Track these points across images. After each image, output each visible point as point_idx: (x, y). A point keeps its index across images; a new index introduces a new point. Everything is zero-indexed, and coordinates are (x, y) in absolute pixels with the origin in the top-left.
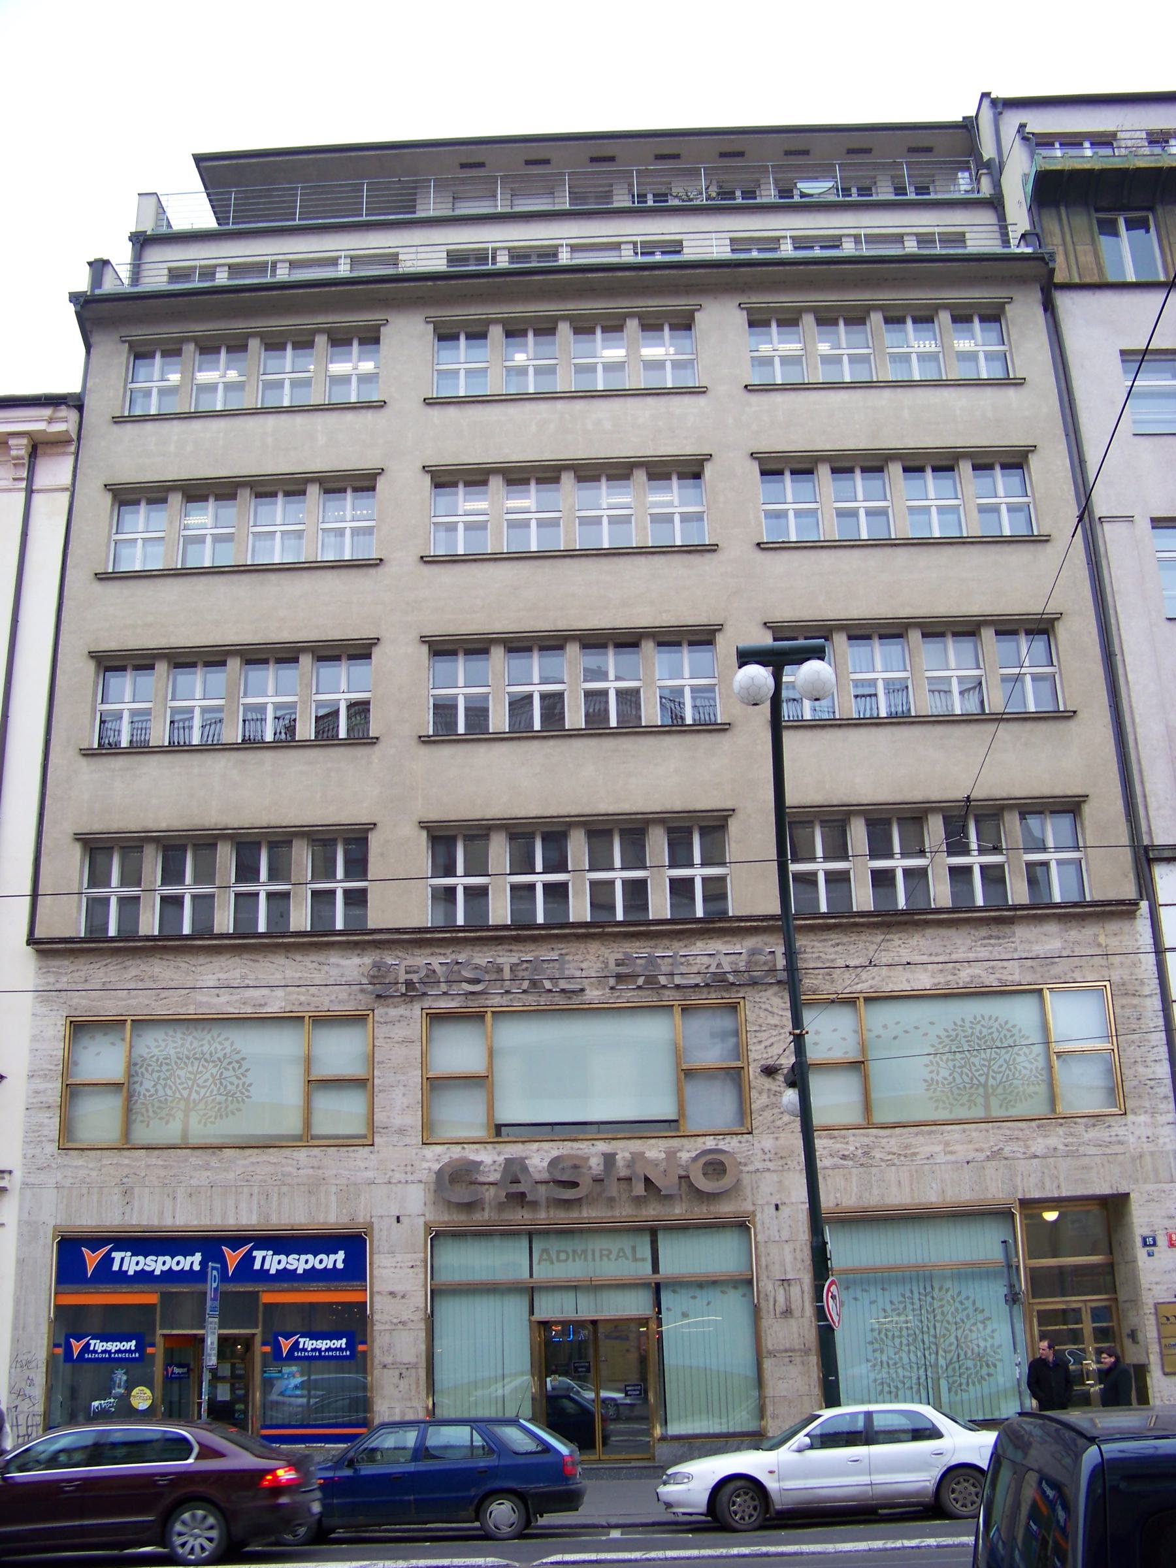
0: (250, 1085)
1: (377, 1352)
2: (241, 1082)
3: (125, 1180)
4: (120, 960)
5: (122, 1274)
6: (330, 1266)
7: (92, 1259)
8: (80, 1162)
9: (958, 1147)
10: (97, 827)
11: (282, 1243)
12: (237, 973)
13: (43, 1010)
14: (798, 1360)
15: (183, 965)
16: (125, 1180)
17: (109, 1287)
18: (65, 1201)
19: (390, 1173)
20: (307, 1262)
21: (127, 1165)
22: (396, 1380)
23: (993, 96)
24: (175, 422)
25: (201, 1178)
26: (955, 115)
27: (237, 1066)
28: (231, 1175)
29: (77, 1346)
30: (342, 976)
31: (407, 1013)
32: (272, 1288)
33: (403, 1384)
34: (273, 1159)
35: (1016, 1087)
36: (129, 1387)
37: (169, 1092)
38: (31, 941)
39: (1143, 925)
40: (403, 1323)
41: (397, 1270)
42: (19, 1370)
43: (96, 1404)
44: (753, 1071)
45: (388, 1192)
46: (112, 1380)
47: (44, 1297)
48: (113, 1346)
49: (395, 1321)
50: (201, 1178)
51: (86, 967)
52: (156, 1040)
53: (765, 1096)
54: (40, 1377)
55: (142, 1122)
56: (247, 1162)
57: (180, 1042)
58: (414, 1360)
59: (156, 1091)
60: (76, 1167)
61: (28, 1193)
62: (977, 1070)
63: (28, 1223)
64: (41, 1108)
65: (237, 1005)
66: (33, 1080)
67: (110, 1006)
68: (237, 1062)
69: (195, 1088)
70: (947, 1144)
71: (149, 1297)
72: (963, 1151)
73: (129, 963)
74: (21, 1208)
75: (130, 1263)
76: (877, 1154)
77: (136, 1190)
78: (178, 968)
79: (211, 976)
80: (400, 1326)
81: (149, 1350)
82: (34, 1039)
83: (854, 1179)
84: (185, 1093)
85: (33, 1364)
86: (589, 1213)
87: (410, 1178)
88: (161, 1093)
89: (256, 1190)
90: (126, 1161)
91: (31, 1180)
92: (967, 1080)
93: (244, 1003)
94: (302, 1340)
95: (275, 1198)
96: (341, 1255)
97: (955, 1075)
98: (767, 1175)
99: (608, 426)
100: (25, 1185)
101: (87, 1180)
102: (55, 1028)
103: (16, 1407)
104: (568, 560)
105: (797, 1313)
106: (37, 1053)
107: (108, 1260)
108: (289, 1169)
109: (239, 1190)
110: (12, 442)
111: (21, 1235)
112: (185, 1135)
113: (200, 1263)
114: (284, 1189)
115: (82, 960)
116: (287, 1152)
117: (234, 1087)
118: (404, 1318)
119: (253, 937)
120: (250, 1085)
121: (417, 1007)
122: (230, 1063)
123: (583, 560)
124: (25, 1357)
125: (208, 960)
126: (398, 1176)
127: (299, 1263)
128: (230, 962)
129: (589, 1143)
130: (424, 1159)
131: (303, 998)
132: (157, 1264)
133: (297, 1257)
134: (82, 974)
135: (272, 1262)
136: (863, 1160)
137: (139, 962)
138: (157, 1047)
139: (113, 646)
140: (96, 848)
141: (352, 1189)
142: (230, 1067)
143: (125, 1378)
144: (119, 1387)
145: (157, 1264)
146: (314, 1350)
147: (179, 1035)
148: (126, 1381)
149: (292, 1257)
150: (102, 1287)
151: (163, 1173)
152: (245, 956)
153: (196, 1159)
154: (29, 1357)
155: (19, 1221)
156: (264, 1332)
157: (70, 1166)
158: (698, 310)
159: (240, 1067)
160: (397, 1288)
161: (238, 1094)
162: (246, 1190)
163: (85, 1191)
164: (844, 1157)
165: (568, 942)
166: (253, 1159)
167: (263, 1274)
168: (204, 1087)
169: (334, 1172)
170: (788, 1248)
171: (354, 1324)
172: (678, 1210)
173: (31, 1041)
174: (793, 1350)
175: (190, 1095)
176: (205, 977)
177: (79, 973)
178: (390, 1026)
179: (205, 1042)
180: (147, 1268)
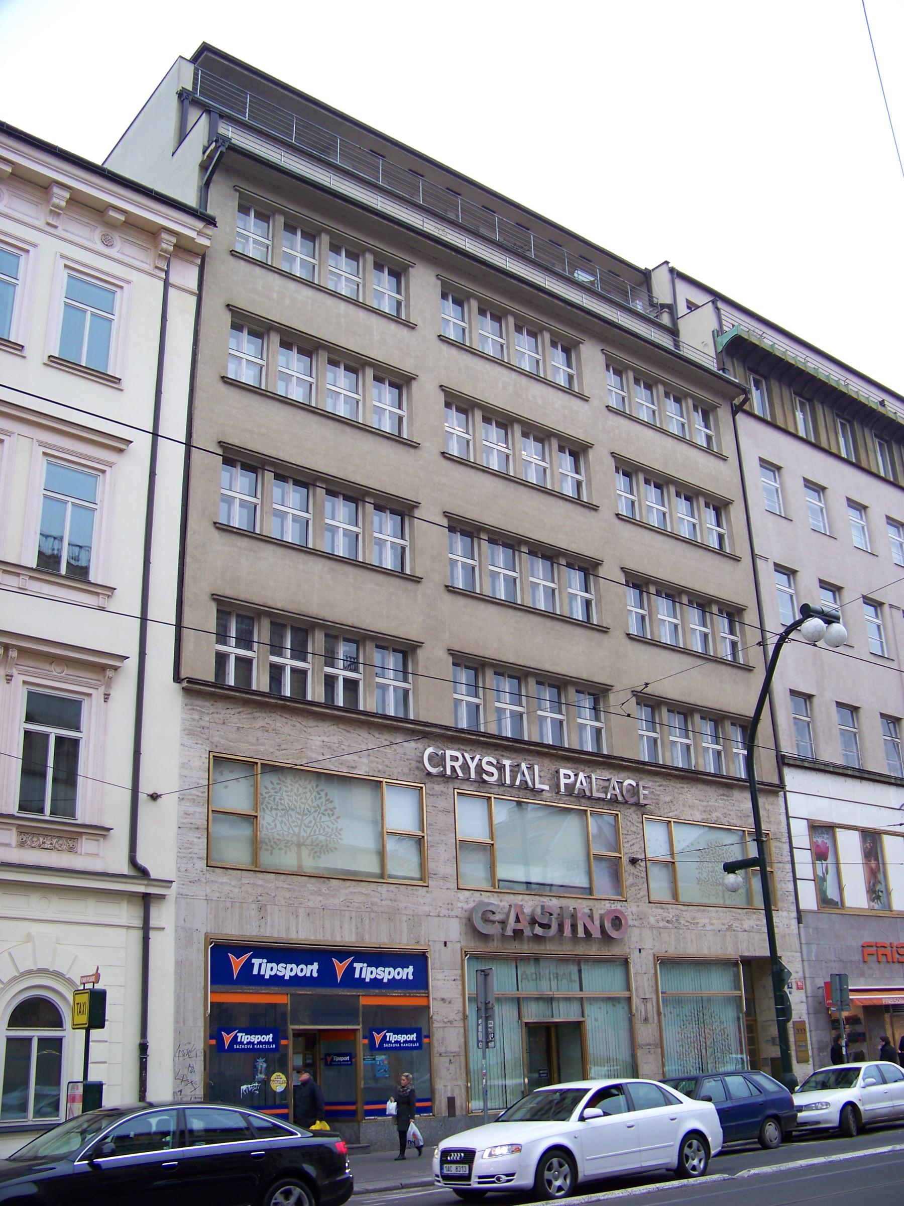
0: (341, 830)
1: (436, 1044)
2: (334, 827)
3: (260, 898)
4: (250, 711)
5: (260, 977)
6: (308, 975)
7: (237, 963)
8: (225, 880)
9: (715, 921)
10: (229, 593)
11: (377, 958)
12: (335, 739)
13: (189, 742)
14: (652, 1051)
15: (297, 724)
16: (260, 898)
17: (252, 989)
18: (213, 912)
19: (439, 909)
20: (291, 970)
21: (262, 886)
22: (447, 1065)
23: (670, 265)
24: (277, 276)
25: (315, 901)
26: (642, 263)
27: (331, 813)
28: (336, 901)
29: (227, 1038)
30: (405, 754)
31: (445, 790)
32: (368, 993)
33: (452, 1068)
34: (364, 891)
35: (321, 842)
36: (269, 1073)
37: (285, 828)
38: (177, 678)
39: (781, 800)
40: (451, 1022)
41: (446, 982)
42: (181, 1058)
43: (244, 1087)
44: (625, 861)
45: (436, 924)
46: (255, 1067)
47: (200, 995)
48: (255, 1039)
49: (446, 1020)
50: (315, 901)
51: (224, 711)
52: (272, 783)
53: (631, 877)
54: (199, 1064)
55: (267, 850)
56: (346, 892)
57: (290, 787)
58: (458, 1050)
59: (276, 826)
60: (222, 883)
61: (183, 902)
62: (293, 822)
63: (184, 929)
64: (191, 829)
65: (337, 764)
66: (183, 803)
67: (244, 750)
68: (331, 810)
69: (303, 827)
70: (710, 919)
71: (281, 998)
72: (717, 924)
73: (257, 715)
74: (177, 915)
75: (266, 968)
76: (682, 921)
77: (269, 907)
78: (294, 726)
79: (317, 738)
80: (449, 1024)
81: (283, 1042)
82: (183, 766)
83: (673, 936)
84: (296, 830)
85: (193, 1054)
86: (550, 948)
87: (452, 914)
88: (279, 828)
89: (354, 914)
90: (261, 882)
91: (185, 891)
92: (285, 828)
93: (341, 764)
94: (239, 1035)
95: (367, 922)
96: (316, 966)
97: (277, 822)
98: (634, 929)
99: (540, 402)
100: (180, 895)
101: (231, 895)
102: (200, 761)
103: (181, 1091)
104: (522, 487)
105: (651, 1021)
106: (186, 779)
107: (249, 965)
108: (375, 900)
109: (343, 913)
110: (56, 190)
111: (178, 939)
112: (300, 867)
113: (318, 971)
114: (373, 915)
115: (220, 705)
116: (373, 886)
117: (330, 830)
118: (451, 1018)
119: (302, 703)
120: (341, 830)
121: (451, 786)
122: (326, 810)
123: (531, 490)
124: (186, 1047)
125: (315, 724)
126: (444, 912)
127: (385, 974)
128: (330, 728)
129: (548, 898)
130: (458, 900)
131: (380, 767)
132: (287, 970)
133: (284, 965)
134: (221, 716)
135: (367, 972)
136: (676, 925)
137: (264, 715)
138: (273, 789)
139: (236, 442)
140: (226, 607)
141: (416, 919)
142: (326, 813)
143: (265, 1065)
144: (261, 1073)
145: (287, 970)
146: (396, 1042)
147: (302, 782)
148: (266, 1068)
149: (380, 968)
150: (246, 988)
151: (288, 895)
152: (341, 726)
153: (312, 885)
154: (190, 1047)
155: (177, 927)
156: (363, 1028)
157: (216, 882)
158: (412, 267)
159: (333, 815)
160: (446, 996)
161: (333, 836)
162: (347, 913)
163: (229, 905)
164: (668, 922)
165: (534, 756)
166: (351, 890)
167: (361, 982)
168: (309, 827)
169: (404, 905)
170: (645, 977)
171: (416, 1021)
172: (594, 950)
173: (181, 767)
174: (650, 1045)
175: (299, 832)
176: (313, 738)
177: (218, 716)
178: (435, 798)
179: (307, 790)
180: (279, 974)
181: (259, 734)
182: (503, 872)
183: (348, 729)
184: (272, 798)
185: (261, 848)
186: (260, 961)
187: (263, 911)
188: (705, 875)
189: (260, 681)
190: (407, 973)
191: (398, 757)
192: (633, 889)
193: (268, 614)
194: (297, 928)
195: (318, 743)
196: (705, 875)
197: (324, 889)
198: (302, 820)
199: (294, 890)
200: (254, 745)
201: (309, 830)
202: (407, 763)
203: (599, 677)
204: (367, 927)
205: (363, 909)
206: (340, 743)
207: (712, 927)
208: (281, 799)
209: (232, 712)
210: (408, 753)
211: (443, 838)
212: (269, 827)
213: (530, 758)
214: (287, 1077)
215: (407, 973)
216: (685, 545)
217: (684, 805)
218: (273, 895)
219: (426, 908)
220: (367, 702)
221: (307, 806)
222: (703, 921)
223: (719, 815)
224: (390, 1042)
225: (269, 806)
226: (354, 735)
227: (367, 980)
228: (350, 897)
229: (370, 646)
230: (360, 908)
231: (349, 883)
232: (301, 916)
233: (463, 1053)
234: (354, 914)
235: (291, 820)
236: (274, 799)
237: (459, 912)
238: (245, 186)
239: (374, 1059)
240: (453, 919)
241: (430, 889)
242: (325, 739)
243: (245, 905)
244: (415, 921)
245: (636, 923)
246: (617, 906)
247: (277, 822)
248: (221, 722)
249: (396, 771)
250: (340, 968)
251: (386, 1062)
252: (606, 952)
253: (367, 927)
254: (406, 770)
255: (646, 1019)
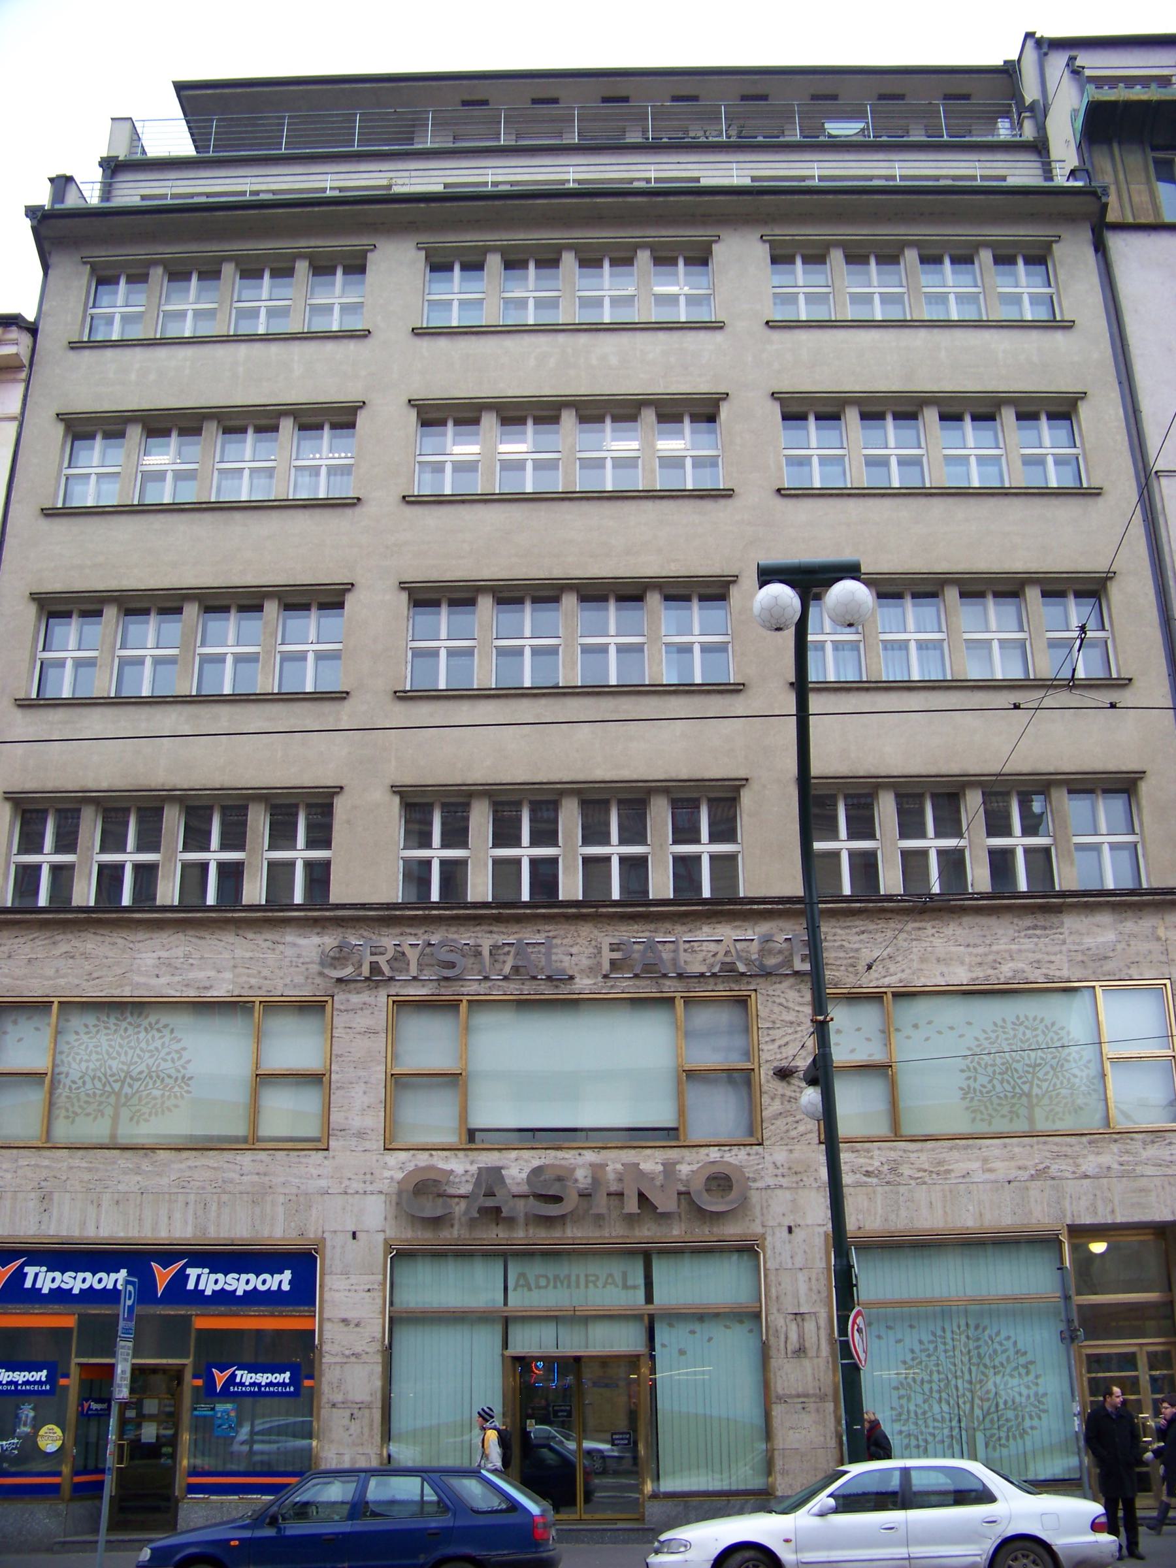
1: (325, 1388)
3: (43, 1184)
4: (48, 934)
6: (110, 1286)
9: (997, 1165)
12: (179, 952)
15: (119, 941)
16: (43, 1184)
17: (21, 1308)
19: (347, 1183)
21: (47, 1167)
22: (346, 1421)
25: (131, 1183)
27: (176, 1056)
28: (165, 1181)
30: (299, 956)
31: (371, 1000)
34: (212, 1163)
36: (37, 1425)
40: (356, 1355)
41: (352, 1294)
44: (765, 1074)
45: (345, 1205)
46: (17, 1416)
49: (347, 1352)
50: (131, 1183)
51: (12, 941)
52: (86, 1026)
56: (183, 1166)
57: (114, 1028)
58: (368, 1398)
59: (994, 1086)
62: (1020, 1078)
68: (177, 1052)
69: (1036, 1081)
72: (1003, 1170)
75: (44, 1279)
76: (906, 1171)
77: (56, 1196)
78: (115, 944)
80: (353, 1359)
81: (63, 1382)
86: (573, 1233)
87: (369, 1188)
89: (192, 1198)
90: (46, 1163)
93: (187, 985)
95: (214, 1207)
97: (995, 1082)
98: (779, 1192)
105: (812, 1352)
108: (232, 1175)
109: (173, 1197)
112: (113, 1136)
113: (290, 1282)
114: (225, 1198)
118: (358, 1349)
125: (147, 936)
126: (356, 1186)
131: (253, 981)
135: (208, 1281)
136: (890, 1177)
137: (70, 936)
139: (58, 587)
143: (32, 1414)
144: (25, 1425)
146: (253, 1384)
148: (34, 1418)
151: (86, 1176)
152: (191, 933)
164: (868, 1174)
166: (190, 1163)
168: (1046, 1080)
169: (282, 1179)
170: (802, 1277)
171: (299, 1355)
172: (676, 1232)
174: (806, 1396)
176: (144, 955)
178: (351, 1014)
181: (61, 963)
182: (481, 1118)
183: (202, 934)
184: (83, 1047)
185: (58, 1117)
186: (199, 1271)
187: (45, 1201)
188: (983, 1080)
189: (979, 877)
190: (284, 1280)
191: (286, 962)
192: (780, 1123)
193: (172, 799)
194: (98, 1221)
195: (150, 962)
196: (983, 1080)
197: (146, 1165)
198: (1034, 1074)
199: (97, 1170)
200: (50, 978)
201: (1045, 1085)
202: (303, 968)
203: (1129, 764)
204: (213, 1214)
205: (209, 1189)
206: (187, 957)
207: (988, 1176)
208: (96, 1047)
209: (22, 940)
210: (304, 954)
211: (362, 1073)
212: (984, 1090)
213: (547, 928)
214: (63, 1432)
215: (284, 1280)
216: (950, 501)
217: (923, 960)
218: (64, 1178)
219: (323, 1183)
220: (1066, 877)
221: (138, 1051)
222: (961, 1167)
223: (1021, 965)
224: (242, 1384)
225: (78, 1058)
226: (210, 942)
227: (208, 1292)
228: (187, 1174)
229: (1060, 796)
230: (204, 1188)
231: (185, 1154)
232: (105, 1205)
233: (378, 1404)
234: (192, 1198)
235: (1016, 1076)
236: (87, 1047)
237: (385, 1186)
238: (424, 238)
239: (213, 1409)
240: (374, 1197)
241: (331, 1153)
242: (164, 954)
243: (20, 1195)
244: (300, 1202)
245: (784, 1182)
246: (737, 1157)
247: (995, 1082)
248: (6, 956)
249: (280, 983)
250: (163, 1276)
251: (233, 1414)
252: (703, 1233)
253: (213, 1214)
254: (299, 979)
255: (801, 1351)
